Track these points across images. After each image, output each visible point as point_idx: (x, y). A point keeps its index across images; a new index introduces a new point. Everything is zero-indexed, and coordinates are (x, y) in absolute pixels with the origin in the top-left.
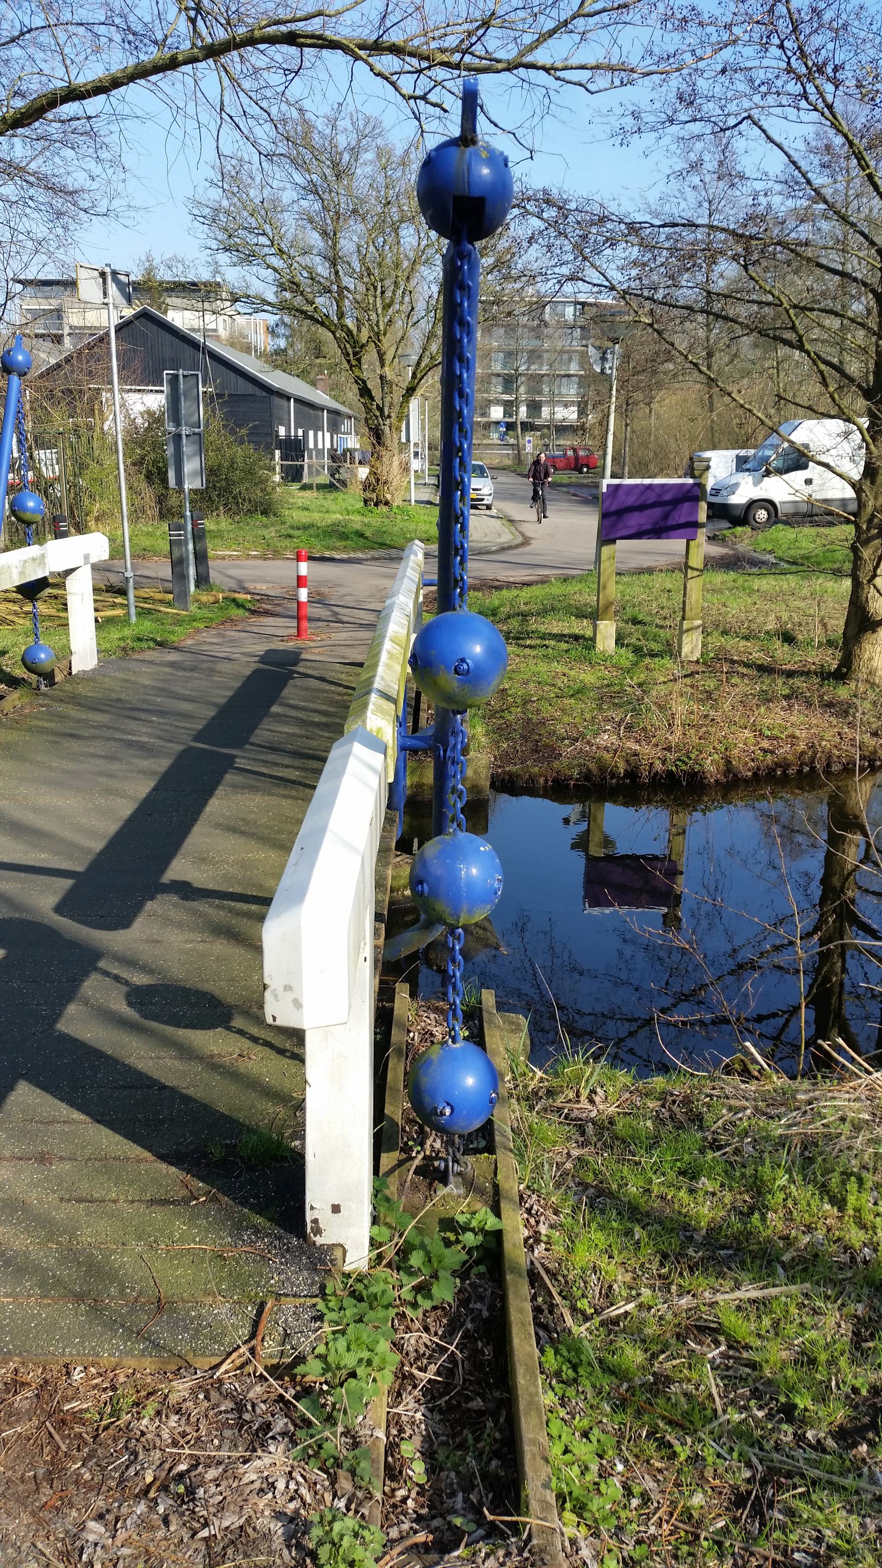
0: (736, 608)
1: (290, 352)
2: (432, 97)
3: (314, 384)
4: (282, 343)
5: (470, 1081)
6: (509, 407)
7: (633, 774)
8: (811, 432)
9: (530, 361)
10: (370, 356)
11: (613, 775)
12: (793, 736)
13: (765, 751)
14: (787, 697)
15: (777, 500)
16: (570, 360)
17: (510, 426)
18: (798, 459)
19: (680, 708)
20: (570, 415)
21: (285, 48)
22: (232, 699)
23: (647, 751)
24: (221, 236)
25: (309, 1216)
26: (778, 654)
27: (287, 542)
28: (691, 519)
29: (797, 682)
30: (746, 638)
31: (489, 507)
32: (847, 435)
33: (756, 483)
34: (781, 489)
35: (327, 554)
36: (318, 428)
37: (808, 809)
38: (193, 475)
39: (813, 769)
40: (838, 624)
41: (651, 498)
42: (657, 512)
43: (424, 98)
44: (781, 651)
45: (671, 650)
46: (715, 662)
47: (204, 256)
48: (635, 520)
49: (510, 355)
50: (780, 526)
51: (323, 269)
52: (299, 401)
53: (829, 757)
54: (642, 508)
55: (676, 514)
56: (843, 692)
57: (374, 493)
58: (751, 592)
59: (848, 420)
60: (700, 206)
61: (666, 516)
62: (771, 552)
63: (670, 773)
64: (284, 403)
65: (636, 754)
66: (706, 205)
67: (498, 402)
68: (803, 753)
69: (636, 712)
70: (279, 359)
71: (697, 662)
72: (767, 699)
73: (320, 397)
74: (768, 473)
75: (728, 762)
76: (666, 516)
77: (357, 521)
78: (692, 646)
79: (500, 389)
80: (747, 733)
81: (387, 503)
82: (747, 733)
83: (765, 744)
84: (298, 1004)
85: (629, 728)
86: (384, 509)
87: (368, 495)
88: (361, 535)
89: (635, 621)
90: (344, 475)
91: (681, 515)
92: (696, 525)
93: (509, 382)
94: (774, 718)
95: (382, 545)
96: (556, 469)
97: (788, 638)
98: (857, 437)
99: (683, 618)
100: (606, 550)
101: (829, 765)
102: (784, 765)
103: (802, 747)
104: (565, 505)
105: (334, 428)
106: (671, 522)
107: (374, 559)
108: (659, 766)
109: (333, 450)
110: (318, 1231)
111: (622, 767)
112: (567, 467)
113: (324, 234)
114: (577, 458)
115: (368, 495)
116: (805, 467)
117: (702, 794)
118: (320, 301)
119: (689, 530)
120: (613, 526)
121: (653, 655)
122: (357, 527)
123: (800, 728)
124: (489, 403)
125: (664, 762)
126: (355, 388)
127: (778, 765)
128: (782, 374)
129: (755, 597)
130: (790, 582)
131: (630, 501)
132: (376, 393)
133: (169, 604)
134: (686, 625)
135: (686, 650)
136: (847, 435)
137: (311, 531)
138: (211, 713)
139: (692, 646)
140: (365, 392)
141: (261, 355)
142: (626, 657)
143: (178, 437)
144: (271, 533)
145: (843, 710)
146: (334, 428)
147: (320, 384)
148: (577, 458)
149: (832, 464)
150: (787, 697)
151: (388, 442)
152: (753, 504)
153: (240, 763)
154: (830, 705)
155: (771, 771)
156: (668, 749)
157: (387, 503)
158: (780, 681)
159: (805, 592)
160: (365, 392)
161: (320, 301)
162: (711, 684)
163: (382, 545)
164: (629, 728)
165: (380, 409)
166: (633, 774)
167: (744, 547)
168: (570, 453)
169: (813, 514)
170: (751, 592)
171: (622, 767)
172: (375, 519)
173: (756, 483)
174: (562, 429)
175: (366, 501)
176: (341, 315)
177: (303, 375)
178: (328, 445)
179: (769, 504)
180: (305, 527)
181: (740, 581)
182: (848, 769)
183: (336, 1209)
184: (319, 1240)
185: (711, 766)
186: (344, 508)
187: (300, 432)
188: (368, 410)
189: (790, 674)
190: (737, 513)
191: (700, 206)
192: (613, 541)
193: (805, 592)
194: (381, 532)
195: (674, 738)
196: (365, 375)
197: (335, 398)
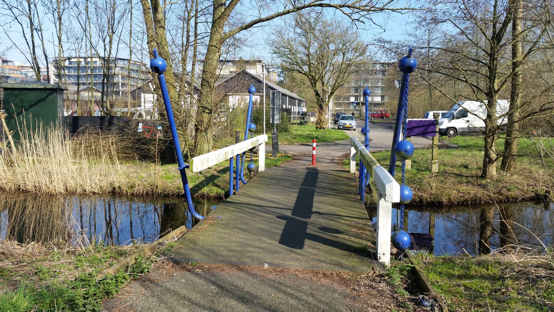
0: (447, 159)
1: (284, 81)
2: (360, 20)
3: (292, 91)
4: (282, 79)
5: (406, 238)
6: (356, 97)
7: (421, 201)
8: (469, 105)
9: (364, 82)
10: (319, 84)
11: (415, 202)
12: (469, 193)
13: (461, 197)
14: (466, 183)
15: (457, 127)
16: (378, 82)
17: (358, 104)
18: (464, 114)
19: (434, 185)
20: (378, 99)
21: (319, 7)
22: (306, 176)
23: (425, 196)
24: (274, 49)
25: (378, 255)
26: (463, 171)
27: (295, 140)
28: (434, 130)
29: (469, 179)
30: (452, 167)
31: (354, 130)
32: (481, 106)
33: (449, 122)
34: (460, 124)
35: (308, 143)
36: (294, 105)
37: (474, 216)
38: (277, 120)
39: (475, 202)
40: (481, 164)
41: (422, 124)
42: (423, 128)
43: (358, 20)
44: (464, 171)
45: (429, 169)
46: (442, 173)
47: (269, 55)
48: (416, 131)
49: (357, 81)
50: (459, 136)
51: (305, 58)
52: (290, 97)
53: (480, 199)
54: (418, 127)
55: (429, 129)
56: (484, 182)
57: (319, 124)
58: (451, 155)
59: (482, 102)
60: (426, 31)
61: (426, 130)
62: (456, 144)
63: (432, 202)
64: (285, 97)
65: (422, 196)
66: (428, 31)
67: (353, 96)
68: (472, 197)
69: (420, 185)
70: (281, 83)
71: (437, 173)
72: (461, 183)
73: (294, 95)
74: (453, 118)
75: (450, 199)
76: (426, 130)
77: (315, 134)
78: (435, 168)
79: (354, 92)
80: (455, 191)
81: (323, 128)
82: (455, 191)
83: (461, 195)
84: (392, 198)
85: (418, 189)
86: (323, 130)
87: (317, 126)
88: (317, 138)
89: (415, 162)
90: (306, 119)
91: (431, 129)
92: (436, 132)
93: (357, 89)
94: (464, 188)
95: (324, 141)
96: (374, 118)
97: (466, 167)
98: (484, 107)
99: (432, 159)
100: (408, 139)
101: (480, 201)
102: (467, 201)
103: (472, 196)
104: (380, 129)
105: (299, 105)
106: (428, 131)
107: (322, 145)
108: (429, 200)
109: (299, 112)
110: (380, 259)
111: (418, 200)
112: (378, 117)
113: (305, 48)
114: (382, 114)
115: (317, 126)
116: (466, 116)
117: (442, 209)
118: (304, 67)
119: (434, 134)
120: (410, 132)
121: (422, 171)
122: (316, 135)
123: (471, 191)
124: (350, 96)
125: (430, 198)
126: (314, 93)
127: (465, 201)
128: (456, 85)
129: (453, 156)
130: (465, 152)
131: (415, 125)
132: (321, 95)
133: (271, 156)
134: (433, 161)
135: (433, 169)
136: (481, 106)
137: (302, 137)
138: (302, 181)
139: (435, 168)
140: (317, 94)
141: (275, 83)
142: (415, 171)
143: (273, 108)
144: (289, 137)
145: (484, 187)
146: (299, 105)
147: (294, 91)
148: (382, 114)
149: (477, 114)
150: (466, 183)
151: (324, 109)
152: (448, 129)
153: (316, 190)
154: (480, 185)
155: (463, 202)
156: (432, 195)
157: (323, 128)
158: (464, 178)
159: (469, 155)
160: (317, 94)
161: (304, 67)
162: (442, 179)
163: (324, 141)
164: (418, 189)
165: (322, 99)
166: (421, 201)
167: (446, 142)
168: (379, 112)
169: (471, 132)
170: (451, 155)
171: (418, 200)
172: (320, 133)
173: (449, 122)
174: (376, 104)
175: (317, 128)
176: (310, 71)
177: (288, 89)
178: (297, 111)
179: (454, 129)
180: (299, 136)
181: (447, 152)
182: (487, 203)
183: (384, 254)
184: (380, 261)
185: (445, 200)
186: (309, 129)
187: (290, 107)
188: (318, 100)
189: (467, 177)
190: (443, 131)
191: (426, 31)
192: (410, 137)
193: (469, 155)
194: (323, 137)
195: (433, 192)
196: (317, 89)
197: (298, 95)
